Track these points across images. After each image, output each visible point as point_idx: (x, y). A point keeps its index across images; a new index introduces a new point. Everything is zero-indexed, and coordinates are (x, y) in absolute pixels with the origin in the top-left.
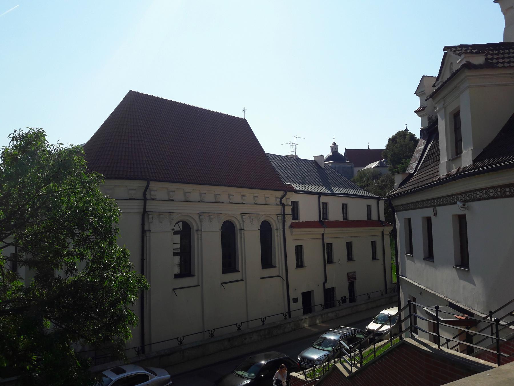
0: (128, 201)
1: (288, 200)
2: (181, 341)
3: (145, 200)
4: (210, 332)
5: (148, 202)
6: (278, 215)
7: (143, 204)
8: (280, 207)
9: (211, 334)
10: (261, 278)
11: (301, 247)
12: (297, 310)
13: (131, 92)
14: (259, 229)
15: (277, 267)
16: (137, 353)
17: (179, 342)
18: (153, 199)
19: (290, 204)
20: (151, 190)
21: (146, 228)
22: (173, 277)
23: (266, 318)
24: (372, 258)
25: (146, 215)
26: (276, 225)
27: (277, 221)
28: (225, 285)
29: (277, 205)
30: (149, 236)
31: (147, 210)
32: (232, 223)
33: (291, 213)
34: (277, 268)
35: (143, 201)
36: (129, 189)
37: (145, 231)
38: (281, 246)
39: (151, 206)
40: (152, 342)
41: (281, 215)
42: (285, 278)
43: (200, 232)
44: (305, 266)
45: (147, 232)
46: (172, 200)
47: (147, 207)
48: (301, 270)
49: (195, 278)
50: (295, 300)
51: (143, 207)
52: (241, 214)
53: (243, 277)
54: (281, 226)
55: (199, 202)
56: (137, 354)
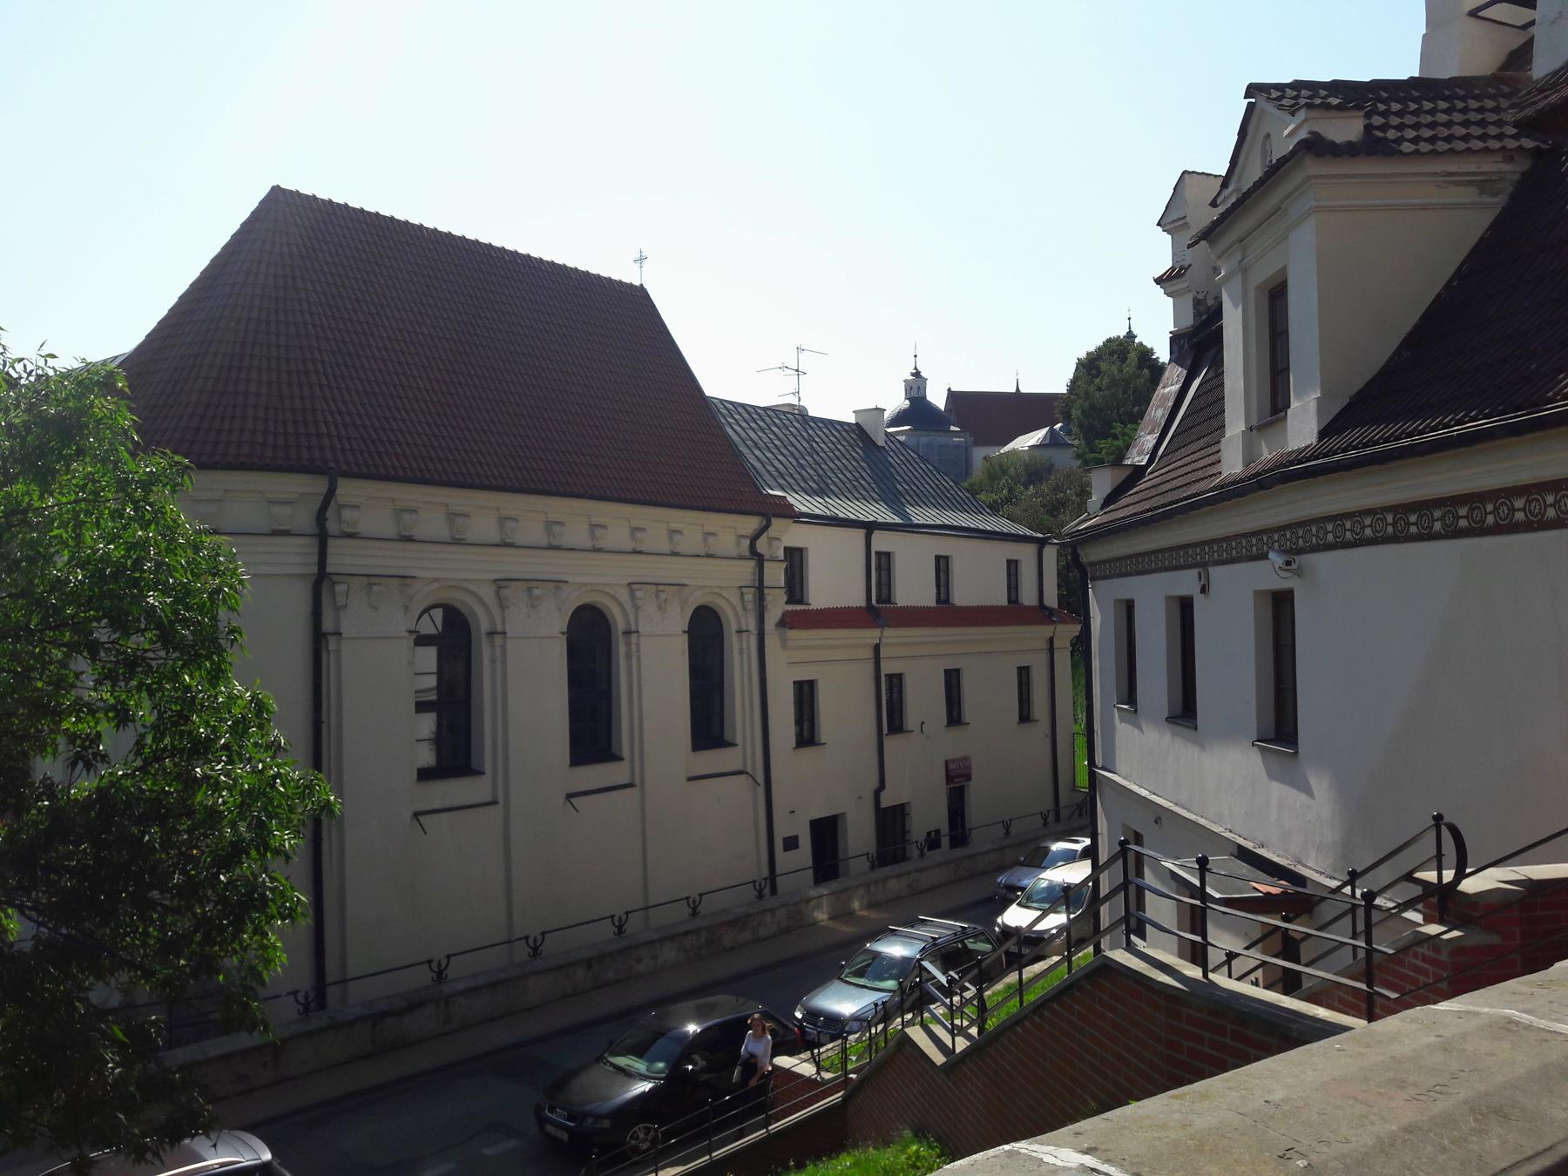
1: (775, 543)
3: (322, 537)
5: (331, 542)
7: (316, 550)
8: (751, 565)
11: (811, 684)
21: (327, 625)
25: (326, 584)
26: (736, 618)
29: (741, 558)
41: (752, 589)
42: (760, 779)
44: (822, 742)
45: (329, 637)
47: (330, 560)
48: (808, 753)
49: (626, 764)
50: (791, 843)
51: (316, 559)
54: (751, 624)
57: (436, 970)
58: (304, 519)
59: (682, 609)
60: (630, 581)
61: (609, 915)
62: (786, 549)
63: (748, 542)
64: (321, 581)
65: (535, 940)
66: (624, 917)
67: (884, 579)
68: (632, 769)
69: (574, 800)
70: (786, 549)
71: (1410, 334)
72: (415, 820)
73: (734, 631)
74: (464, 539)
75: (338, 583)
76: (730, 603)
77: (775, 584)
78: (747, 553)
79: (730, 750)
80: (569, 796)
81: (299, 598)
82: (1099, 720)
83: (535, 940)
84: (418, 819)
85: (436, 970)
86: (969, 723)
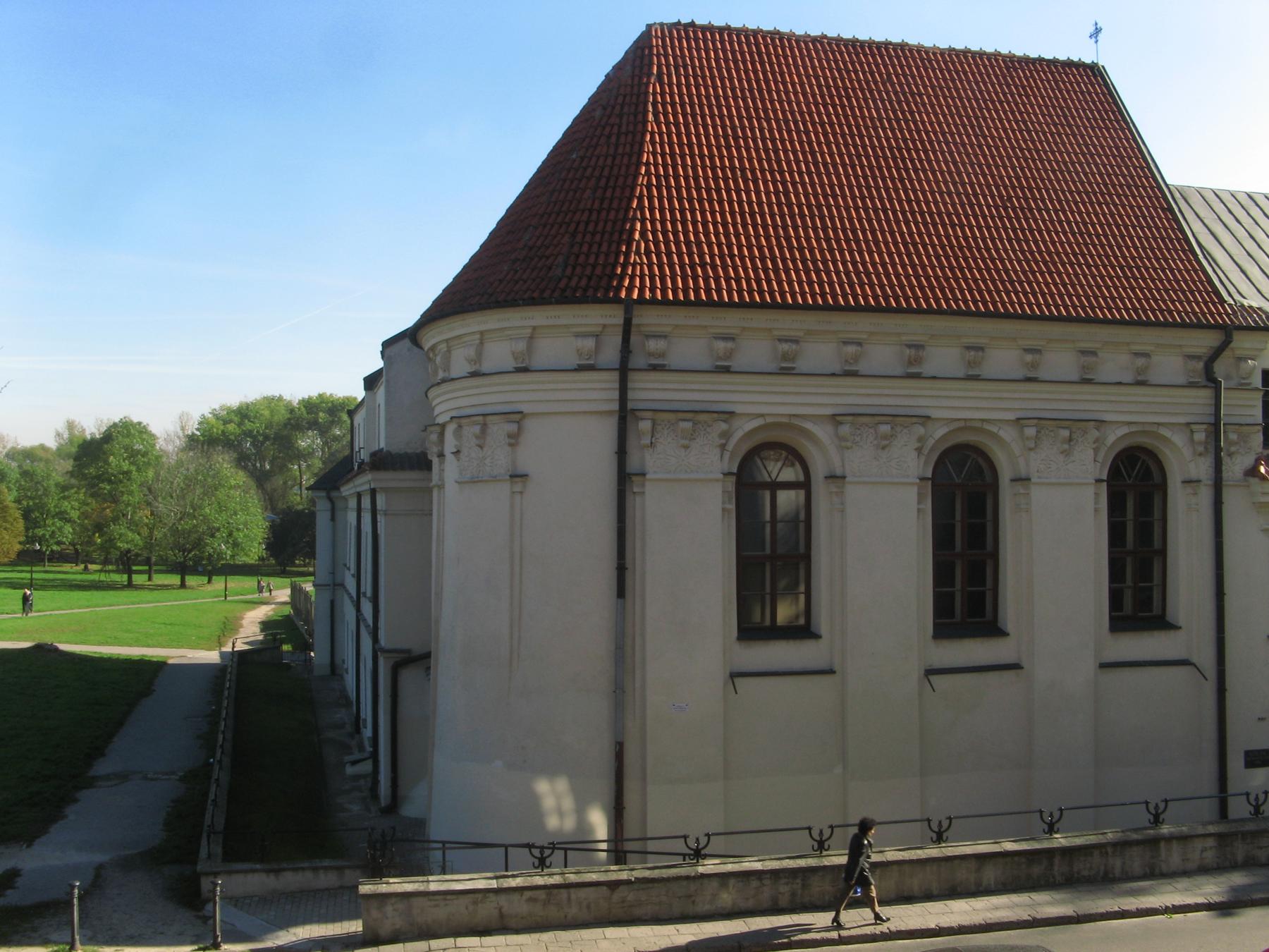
0: (963, 383)
2: (1156, 812)
3: (624, 370)
4: (1252, 798)
5: (632, 376)
6: (1194, 427)
7: (617, 385)
9: (538, 858)
12: (968, 817)
15: (1180, 628)
16: (1152, 818)
17: (934, 832)
18: (655, 368)
19: (1257, 381)
21: (633, 464)
23: (1169, 803)
28: (739, 682)
29: (1191, 385)
31: (630, 405)
33: (1259, 419)
34: (1180, 633)
35: (615, 376)
36: (845, 343)
37: (629, 474)
39: (602, 389)
41: (1205, 426)
42: (1211, 672)
45: (634, 478)
47: (631, 395)
49: (823, 644)
51: (616, 395)
52: (1018, 419)
55: (833, 375)
56: (1152, 821)
57: (936, 830)
58: (611, 353)
60: (1018, 416)
61: (1244, 792)
64: (625, 416)
65: (821, 833)
66: (1162, 806)
69: (933, 678)
72: (926, 680)
74: (979, 375)
75: (642, 419)
77: (1249, 420)
78: (1201, 380)
79: (1172, 633)
81: (605, 432)
83: (821, 833)
84: (929, 680)
85: (936, 830)
86: (1180, 628)
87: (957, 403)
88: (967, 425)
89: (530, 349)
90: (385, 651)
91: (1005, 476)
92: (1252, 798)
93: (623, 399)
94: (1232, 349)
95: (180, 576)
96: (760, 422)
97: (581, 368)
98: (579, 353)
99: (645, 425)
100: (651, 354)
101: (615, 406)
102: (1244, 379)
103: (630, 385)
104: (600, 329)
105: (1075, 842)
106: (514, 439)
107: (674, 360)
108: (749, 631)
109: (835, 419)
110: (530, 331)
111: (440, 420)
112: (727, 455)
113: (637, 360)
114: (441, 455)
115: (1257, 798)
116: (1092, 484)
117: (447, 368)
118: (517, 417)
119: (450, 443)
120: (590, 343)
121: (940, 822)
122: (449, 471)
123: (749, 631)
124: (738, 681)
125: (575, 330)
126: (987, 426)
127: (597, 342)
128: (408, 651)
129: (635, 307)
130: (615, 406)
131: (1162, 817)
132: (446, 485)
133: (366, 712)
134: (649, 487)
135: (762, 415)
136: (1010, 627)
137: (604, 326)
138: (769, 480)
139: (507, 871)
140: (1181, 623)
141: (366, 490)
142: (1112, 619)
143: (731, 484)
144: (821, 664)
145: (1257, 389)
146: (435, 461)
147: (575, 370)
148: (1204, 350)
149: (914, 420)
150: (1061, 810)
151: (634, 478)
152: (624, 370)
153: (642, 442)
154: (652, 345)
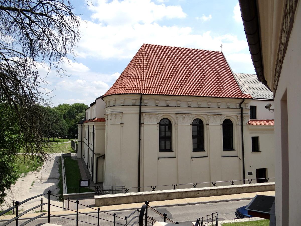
1: (246, 105)
3: (140, 106)
4: (249, 180)
5: (142, 107)
7: (139, 108)
8: (240, 110)
10: (222, 157)
11: (257, 138)
13: (221, 55)
14: (221, 125)
18: (145, 105)
19: (249, 108)
20: (144, 100)
21: (142, 122)
22: (252, 151)
24: (252, 150)
25: (141, 114)
26: (236, 122)
27: (236, 120)
29: (237, 108)
30: (143, 127)
31: (141, 112)
32: (232, 122)
33: (249, 114)
35: (139, 107)
38: (239, 136)
39: (136, 109)
40: (144, 186)
43: (208, 126)
44: (260, 151)
46: (190, 107)
47: (141, 110)
48: (256, 154)
50: (250, 173)
53: (208, 155)
54: (240, 123)
58: (138, 103)
59: (220, 120)
62: (250, 106)
63: (239, 105)
64: (140, 114)
67: (189, 194)
68: (208, 153)
70: (250, 106)
71: (233, 137)
73: (173, 124)
74: (169, 106)
76: (226, 117)
78: (239, 107)
80: (192, 158)
82: (260, 124)
87: (170, 111)
88: (198, 115)
89: (115, 102)
90: (95, 154)
91: (205, 124)
92: (249, 180)
93: (140, 111)
94: (143, 98)
95: (164, 141)
96: (163, 115)
97: (133, 105)
98: (133, 103)
99: (144, 115)
100: (145, 103)
101: (139, 112)
102: (178, 105)
103: (141, 108)
104: (136, 99)
105: (135, 194)
106: (121, 117)
107: (148, 104)
108: (161, 150)
109: (176, 114)
110: (115, 99)
111: (108, 113)
112: (158, 120)
113: (143, 104)
114: (107, 119)
115: (250, 181)
116: (120, 124)
117: (109, 104)
118: (122, 113)
119: (109, 117)
120: (135, 101)
121: (127, 189)
122: (109, 123)
123: (161, 150)
124: (159, 159)
125: (132, 99)
126: (232, 116)
127: (136, 101)
128: (100, 154)
129: (143, 95)
130: (139, 112)
131: (128, 191)
132: (108, 125)
133: (90, 165)
134: (145, 126)
135: (164, 114)
136: (206, 150)
137: (137, 98)
138: (164, 124)
139: (139, 191)
140: (236, 149)
141: (92, 125)
142: (160, 150)
143: (158, 125)
144: (206, 156)
145: (248, 109)
146: (106, 120)
147: (132, 106)
148: (239, 102)
149: (189, 114)
150: (176, 185)
151: (142, 124)
152: (140, 106)
153: (143, 118)
154: (145, 101)
